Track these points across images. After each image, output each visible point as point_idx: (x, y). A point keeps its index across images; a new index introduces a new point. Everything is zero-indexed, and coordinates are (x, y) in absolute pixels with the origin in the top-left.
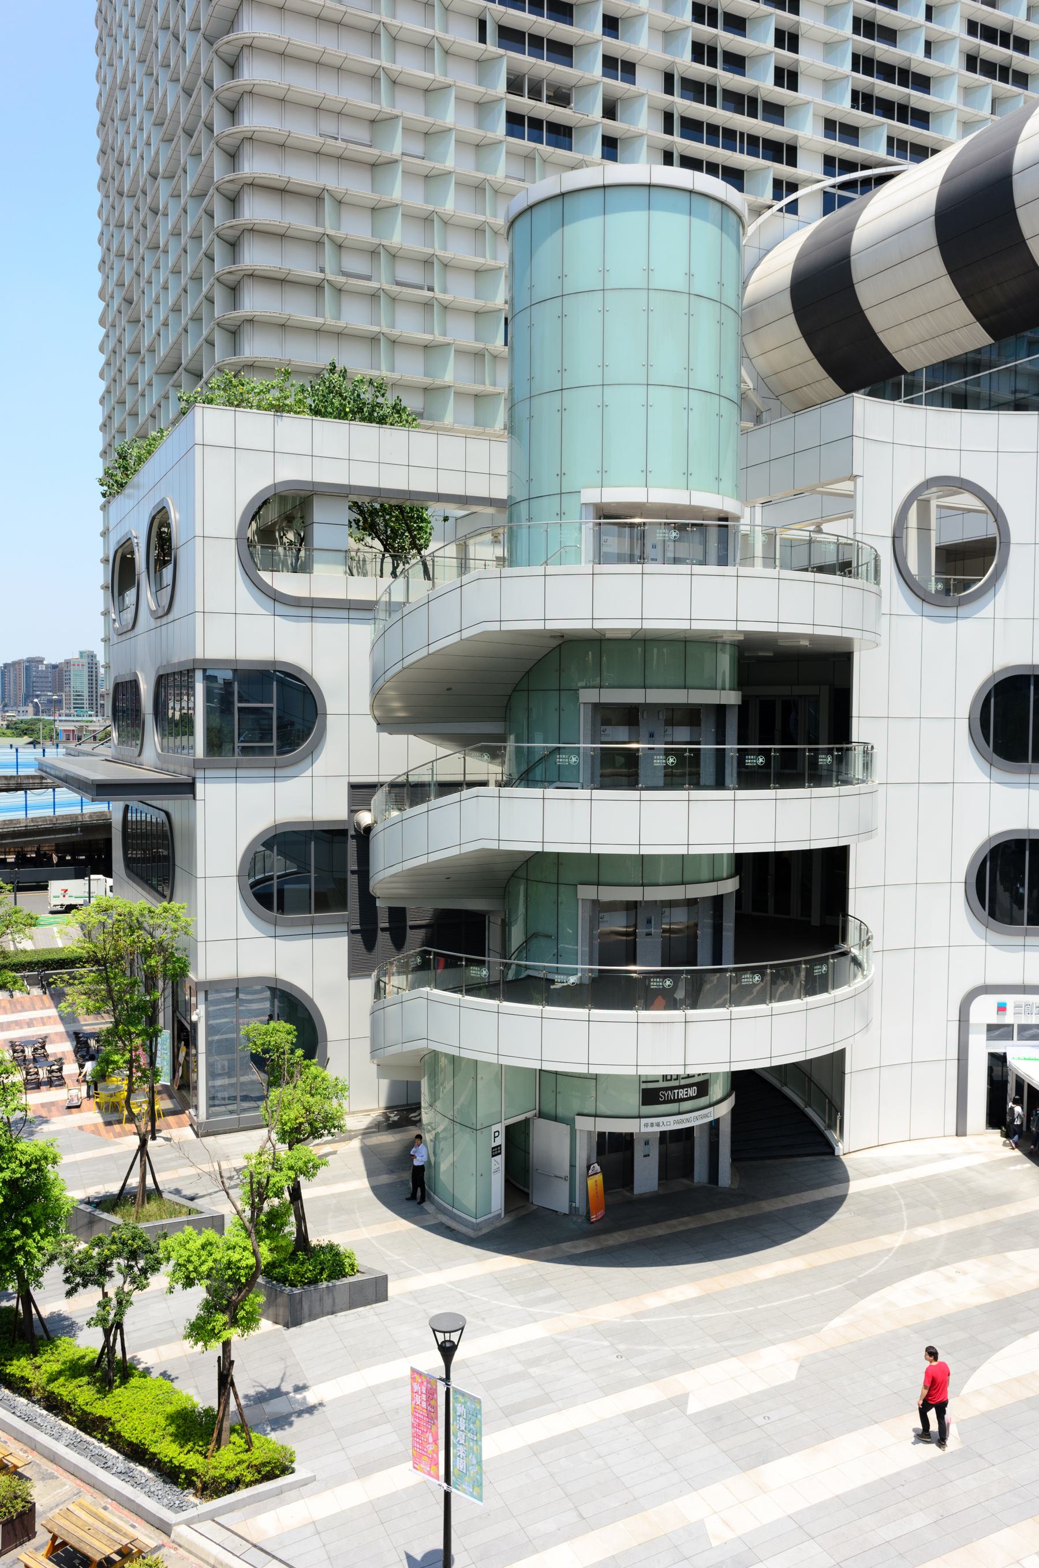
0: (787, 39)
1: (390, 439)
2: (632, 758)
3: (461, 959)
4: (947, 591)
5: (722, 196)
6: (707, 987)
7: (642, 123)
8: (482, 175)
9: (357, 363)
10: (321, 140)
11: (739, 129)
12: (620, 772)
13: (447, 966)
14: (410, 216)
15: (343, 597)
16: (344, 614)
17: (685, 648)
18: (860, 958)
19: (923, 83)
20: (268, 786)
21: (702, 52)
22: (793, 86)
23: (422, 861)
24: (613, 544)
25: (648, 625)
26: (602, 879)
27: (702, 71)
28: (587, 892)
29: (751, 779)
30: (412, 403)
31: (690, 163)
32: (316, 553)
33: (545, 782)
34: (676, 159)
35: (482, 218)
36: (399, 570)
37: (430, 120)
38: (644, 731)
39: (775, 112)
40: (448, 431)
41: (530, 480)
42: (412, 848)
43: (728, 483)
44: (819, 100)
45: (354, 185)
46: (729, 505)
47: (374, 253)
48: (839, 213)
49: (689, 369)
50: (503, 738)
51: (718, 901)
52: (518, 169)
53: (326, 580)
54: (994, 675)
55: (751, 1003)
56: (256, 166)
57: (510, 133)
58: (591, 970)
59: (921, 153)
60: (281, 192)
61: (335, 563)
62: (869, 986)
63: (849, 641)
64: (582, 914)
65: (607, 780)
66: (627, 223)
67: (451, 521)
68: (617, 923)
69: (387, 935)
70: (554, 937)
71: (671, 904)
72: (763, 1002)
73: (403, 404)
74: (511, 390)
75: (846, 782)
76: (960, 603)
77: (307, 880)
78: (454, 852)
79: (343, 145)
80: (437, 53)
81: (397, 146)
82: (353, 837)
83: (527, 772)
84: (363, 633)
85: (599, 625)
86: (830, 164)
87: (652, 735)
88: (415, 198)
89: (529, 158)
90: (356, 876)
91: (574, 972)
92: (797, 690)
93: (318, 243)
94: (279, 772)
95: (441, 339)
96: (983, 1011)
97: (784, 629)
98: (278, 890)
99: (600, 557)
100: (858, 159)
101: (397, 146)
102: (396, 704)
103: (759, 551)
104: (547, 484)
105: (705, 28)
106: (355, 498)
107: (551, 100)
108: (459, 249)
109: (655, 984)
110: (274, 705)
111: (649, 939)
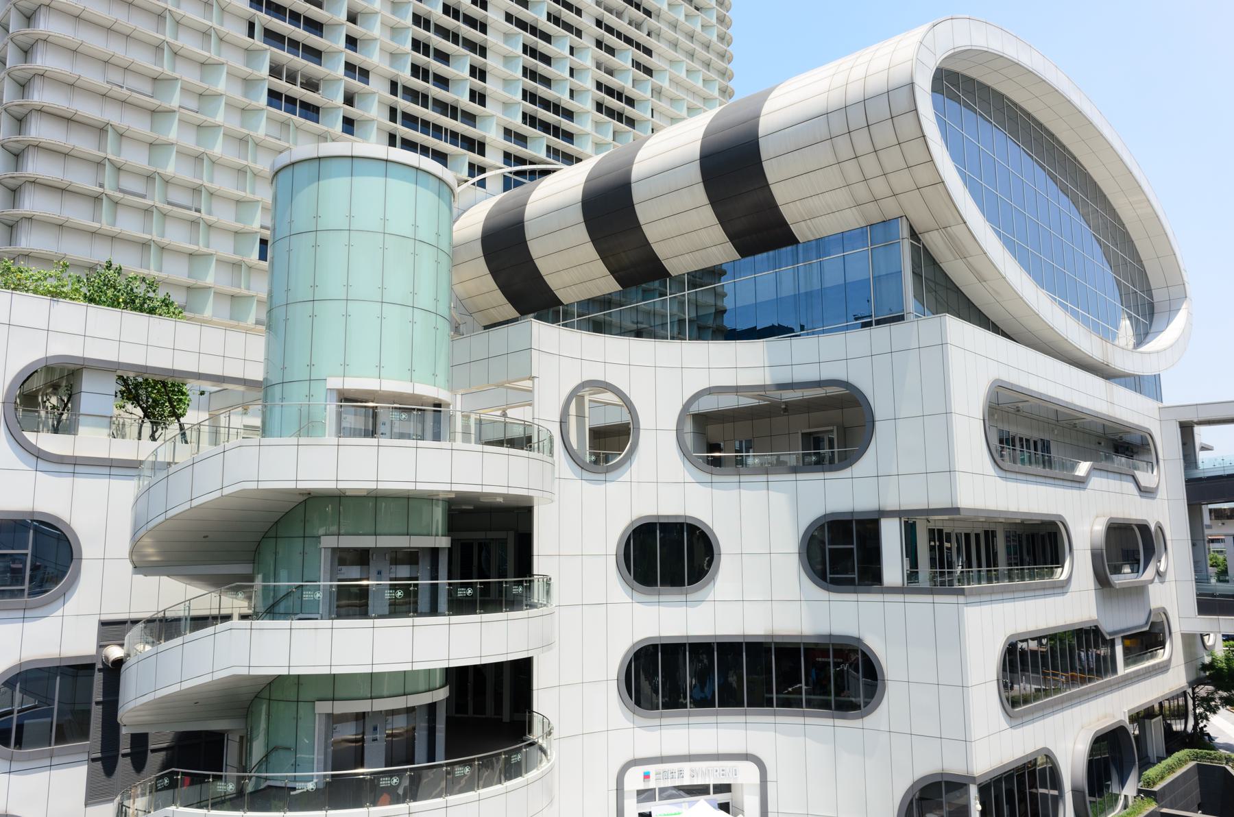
0: (478, 73)
1: (160, 327)
2: (364, 592)
3: (208, 776)
4: (596, 462)
5: (440, 174)
6: (425, 781)
7: (373, 111)
8: (246, 132)
9: (129, 263)
10: (109, 86)
11: (444, 126)
12: (353, 604)
13: (192, 783)
14: (183, 153)
15: (70, 453)
16: (106, 470)
17: (407, 504)
18: (544, 746)
19: (569, 115)
20: (16, 627)
21: (416, 70)
22: (482, 102)
23: (175, 688)
24: (351, 420)
25: (382, 486)
26: (336, 696)
27: (418, 84)
28: (323, 708)
29: (460, 606)
30: (178, 298)
31: (409, 145)
32: (81, 418)
33: (286, 615)
34: (398, 142)
35: (245, 163)
36: (157, 435)
37: (206, 86)
38: (373, 570)
39: (470, 118)
40: (204, 322)
41: (284, 368)
42: (160, 681)
43: (441, 378)
44: (500, 115)
45: (137, 125)
46: (442, 395)
47: (150, 178)
48: (514, 191)
49: (414, 293)
50: (251, 578)
51: (432, 707)
52: (275, 131)
53: (90, 440)
54: (632, 523)
55: (460, 792)
56: (41, 96)
57: (270, 104)
58: (325, 776)
59: (570, 159)
60: (68, 120)
61: (103, 427)
62: (552, 768)
63: (530, 498)
64: (319, 727)
65: (343, 611)
66: (369, 185)
67: (207, 394)
68: (348, 732)
69: (128, 760)
70: (293, 749)
71: (393, 712)
72: (472, 789)
73: (172, 299)
74: (270, 295)
75: (532, 606)
76: (607, 471)
77: (49, 713)
78: (207, 679)
79: (128, 93)
80: (214, 39)
81: (175, 100)
82: (100, 670)
83: (273, 606)
84: (125, 490)
85: (341, 486)
86: (508, 157)
87: (379, 573)
88: (189, 141)
89: (285, 125)
90: (100, 707)
91: (310, 779)
92: (492, 535)
93: (99, 164)
94: (28, 613)
95: (205, 250)
96: (634, 780)
97: (487, 490)
98: (18, 726)
99: (341, 431)
100: (527, 158)
101: (175, 100)
102: (150, 550)
103: (459, 426)
104: (298, 370)
105: (421, 56)
106: (120, 373)
107: (303, 86)
108: (224, 183)
109: (384, 782)
110: (29, 551)
111: (375, 743)
